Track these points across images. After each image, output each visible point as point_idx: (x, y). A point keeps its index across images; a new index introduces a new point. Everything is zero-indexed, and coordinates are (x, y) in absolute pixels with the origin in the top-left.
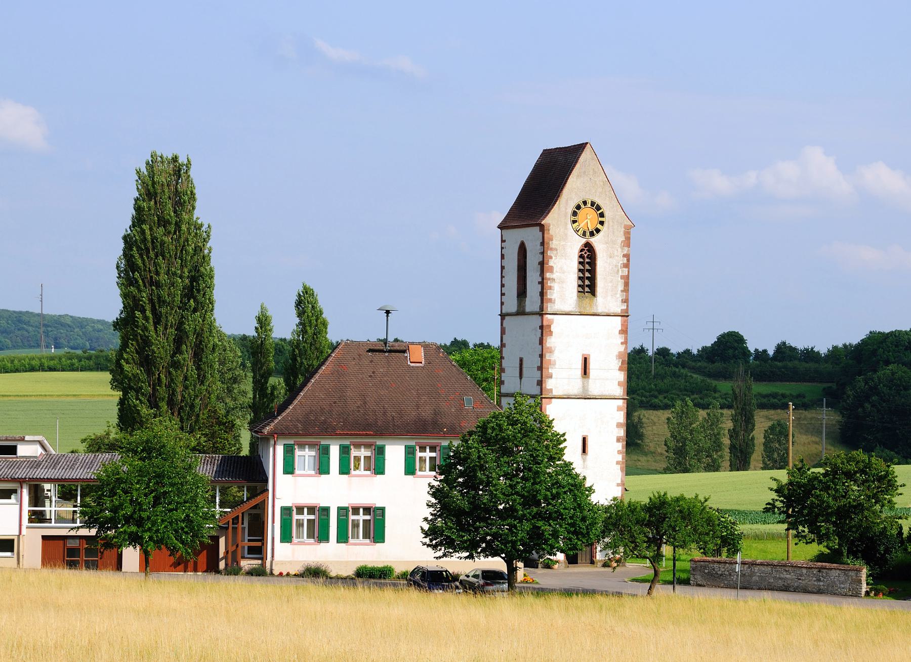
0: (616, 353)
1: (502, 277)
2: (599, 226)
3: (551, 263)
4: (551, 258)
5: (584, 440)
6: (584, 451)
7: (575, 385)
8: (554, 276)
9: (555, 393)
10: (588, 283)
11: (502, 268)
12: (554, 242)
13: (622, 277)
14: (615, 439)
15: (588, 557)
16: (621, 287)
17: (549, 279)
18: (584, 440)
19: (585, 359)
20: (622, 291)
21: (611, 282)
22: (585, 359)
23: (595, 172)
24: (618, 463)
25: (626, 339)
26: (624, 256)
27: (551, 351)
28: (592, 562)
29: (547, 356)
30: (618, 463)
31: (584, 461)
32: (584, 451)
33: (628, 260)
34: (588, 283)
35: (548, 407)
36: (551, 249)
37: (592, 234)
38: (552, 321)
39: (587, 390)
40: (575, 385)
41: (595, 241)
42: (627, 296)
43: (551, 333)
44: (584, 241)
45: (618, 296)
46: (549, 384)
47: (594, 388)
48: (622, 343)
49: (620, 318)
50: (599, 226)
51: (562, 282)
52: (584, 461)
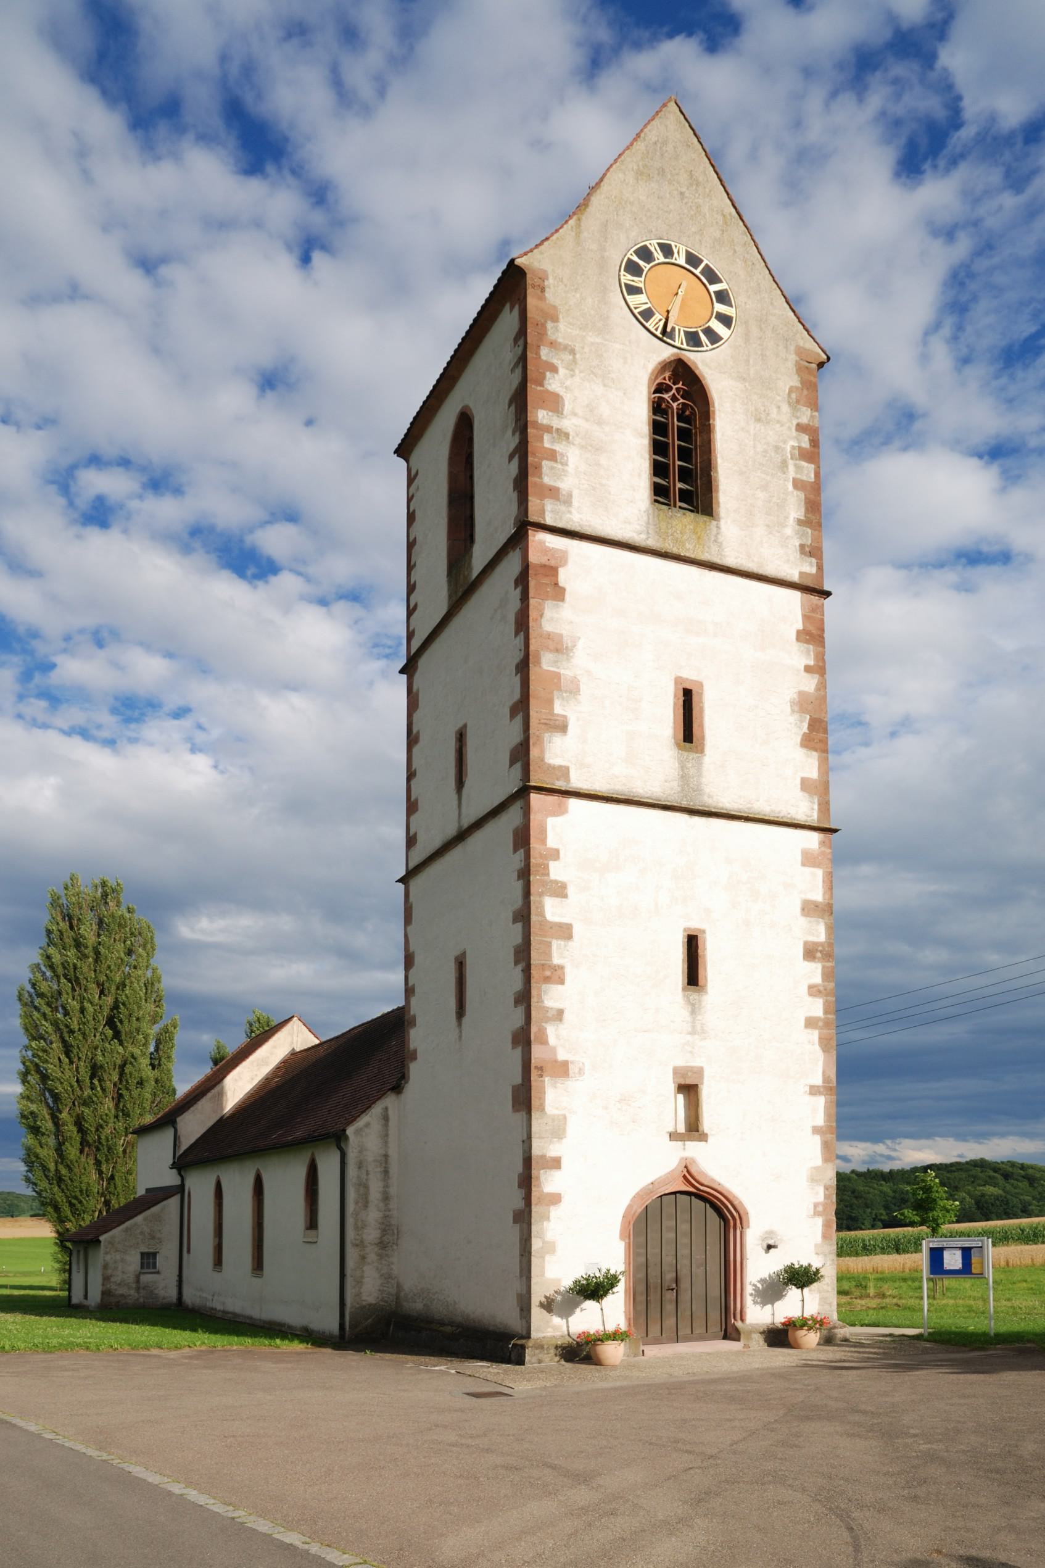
0: (790, 694)
1: (410, 567)
2: (639, 301)
3: (553, 384)
4: (554, 369)
5: (692, 944)
6: (693, 977)
7: (656, 766)
8: (567, 424)
9: (576, 782)
10: (683, 467)
11: (411, 545)
12: (562, 326)
13: (798, 484)
14: (800, 951)
15: (715, 1315)
16: (795, 510)
17: (548, 429)
18: (692, 944)
19: (688, 694)
20: (800, 522)
21: (765, 487)
22: (688, 694)
23: (694, 182)
24: (810, 1023)
25: (821, 658)
26: (800, 428)
27: (560, 648)
28: (730, 1333)
29: (545, 663)
30: (810, 1023)
31: (694, 1009)
32: (693, 977)
33: (815, 443)
34: (683, 467)
35: (552, 823)
36: (552, 344)
37: (693, 339)
38: (563, 557)
39: (698, 790)
40: (656, 766)
41: (703, 361)
42: (818, 539)
43: (558, 593)
44: (666, 353)
45: (789, 531)
46: (555, 752)
47: (721, 779)
48: (808, 669)
49: (797, 594)
50: (639, 301)
51: (594, 448)
52: (694, 1009)
